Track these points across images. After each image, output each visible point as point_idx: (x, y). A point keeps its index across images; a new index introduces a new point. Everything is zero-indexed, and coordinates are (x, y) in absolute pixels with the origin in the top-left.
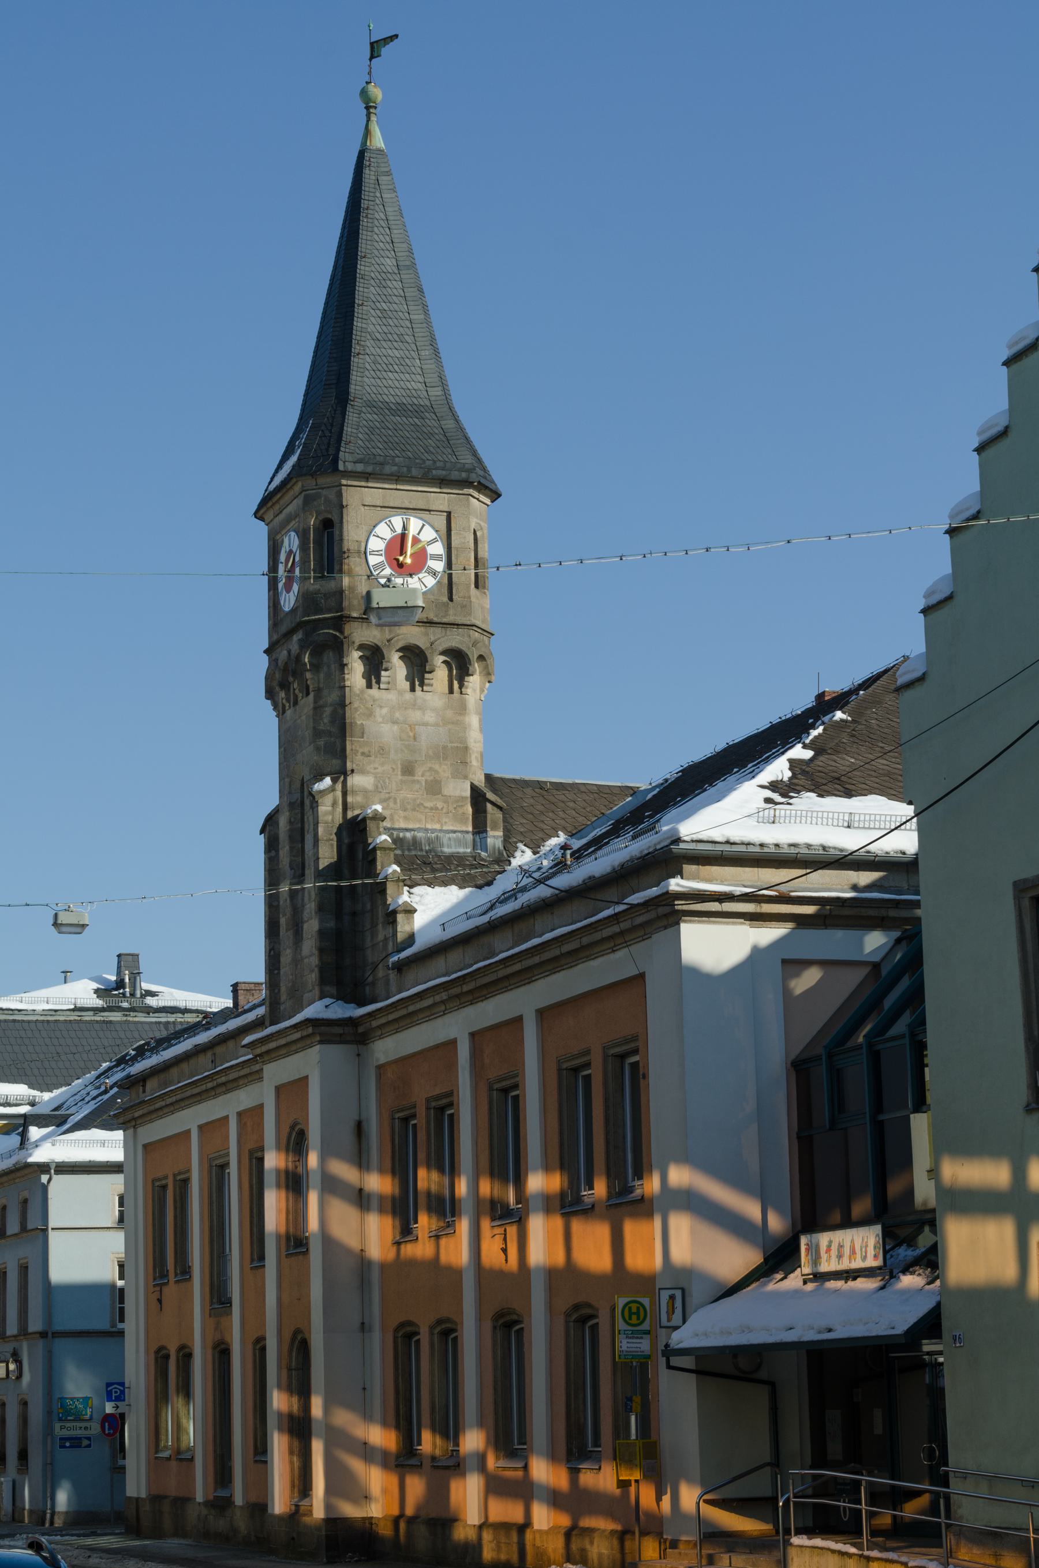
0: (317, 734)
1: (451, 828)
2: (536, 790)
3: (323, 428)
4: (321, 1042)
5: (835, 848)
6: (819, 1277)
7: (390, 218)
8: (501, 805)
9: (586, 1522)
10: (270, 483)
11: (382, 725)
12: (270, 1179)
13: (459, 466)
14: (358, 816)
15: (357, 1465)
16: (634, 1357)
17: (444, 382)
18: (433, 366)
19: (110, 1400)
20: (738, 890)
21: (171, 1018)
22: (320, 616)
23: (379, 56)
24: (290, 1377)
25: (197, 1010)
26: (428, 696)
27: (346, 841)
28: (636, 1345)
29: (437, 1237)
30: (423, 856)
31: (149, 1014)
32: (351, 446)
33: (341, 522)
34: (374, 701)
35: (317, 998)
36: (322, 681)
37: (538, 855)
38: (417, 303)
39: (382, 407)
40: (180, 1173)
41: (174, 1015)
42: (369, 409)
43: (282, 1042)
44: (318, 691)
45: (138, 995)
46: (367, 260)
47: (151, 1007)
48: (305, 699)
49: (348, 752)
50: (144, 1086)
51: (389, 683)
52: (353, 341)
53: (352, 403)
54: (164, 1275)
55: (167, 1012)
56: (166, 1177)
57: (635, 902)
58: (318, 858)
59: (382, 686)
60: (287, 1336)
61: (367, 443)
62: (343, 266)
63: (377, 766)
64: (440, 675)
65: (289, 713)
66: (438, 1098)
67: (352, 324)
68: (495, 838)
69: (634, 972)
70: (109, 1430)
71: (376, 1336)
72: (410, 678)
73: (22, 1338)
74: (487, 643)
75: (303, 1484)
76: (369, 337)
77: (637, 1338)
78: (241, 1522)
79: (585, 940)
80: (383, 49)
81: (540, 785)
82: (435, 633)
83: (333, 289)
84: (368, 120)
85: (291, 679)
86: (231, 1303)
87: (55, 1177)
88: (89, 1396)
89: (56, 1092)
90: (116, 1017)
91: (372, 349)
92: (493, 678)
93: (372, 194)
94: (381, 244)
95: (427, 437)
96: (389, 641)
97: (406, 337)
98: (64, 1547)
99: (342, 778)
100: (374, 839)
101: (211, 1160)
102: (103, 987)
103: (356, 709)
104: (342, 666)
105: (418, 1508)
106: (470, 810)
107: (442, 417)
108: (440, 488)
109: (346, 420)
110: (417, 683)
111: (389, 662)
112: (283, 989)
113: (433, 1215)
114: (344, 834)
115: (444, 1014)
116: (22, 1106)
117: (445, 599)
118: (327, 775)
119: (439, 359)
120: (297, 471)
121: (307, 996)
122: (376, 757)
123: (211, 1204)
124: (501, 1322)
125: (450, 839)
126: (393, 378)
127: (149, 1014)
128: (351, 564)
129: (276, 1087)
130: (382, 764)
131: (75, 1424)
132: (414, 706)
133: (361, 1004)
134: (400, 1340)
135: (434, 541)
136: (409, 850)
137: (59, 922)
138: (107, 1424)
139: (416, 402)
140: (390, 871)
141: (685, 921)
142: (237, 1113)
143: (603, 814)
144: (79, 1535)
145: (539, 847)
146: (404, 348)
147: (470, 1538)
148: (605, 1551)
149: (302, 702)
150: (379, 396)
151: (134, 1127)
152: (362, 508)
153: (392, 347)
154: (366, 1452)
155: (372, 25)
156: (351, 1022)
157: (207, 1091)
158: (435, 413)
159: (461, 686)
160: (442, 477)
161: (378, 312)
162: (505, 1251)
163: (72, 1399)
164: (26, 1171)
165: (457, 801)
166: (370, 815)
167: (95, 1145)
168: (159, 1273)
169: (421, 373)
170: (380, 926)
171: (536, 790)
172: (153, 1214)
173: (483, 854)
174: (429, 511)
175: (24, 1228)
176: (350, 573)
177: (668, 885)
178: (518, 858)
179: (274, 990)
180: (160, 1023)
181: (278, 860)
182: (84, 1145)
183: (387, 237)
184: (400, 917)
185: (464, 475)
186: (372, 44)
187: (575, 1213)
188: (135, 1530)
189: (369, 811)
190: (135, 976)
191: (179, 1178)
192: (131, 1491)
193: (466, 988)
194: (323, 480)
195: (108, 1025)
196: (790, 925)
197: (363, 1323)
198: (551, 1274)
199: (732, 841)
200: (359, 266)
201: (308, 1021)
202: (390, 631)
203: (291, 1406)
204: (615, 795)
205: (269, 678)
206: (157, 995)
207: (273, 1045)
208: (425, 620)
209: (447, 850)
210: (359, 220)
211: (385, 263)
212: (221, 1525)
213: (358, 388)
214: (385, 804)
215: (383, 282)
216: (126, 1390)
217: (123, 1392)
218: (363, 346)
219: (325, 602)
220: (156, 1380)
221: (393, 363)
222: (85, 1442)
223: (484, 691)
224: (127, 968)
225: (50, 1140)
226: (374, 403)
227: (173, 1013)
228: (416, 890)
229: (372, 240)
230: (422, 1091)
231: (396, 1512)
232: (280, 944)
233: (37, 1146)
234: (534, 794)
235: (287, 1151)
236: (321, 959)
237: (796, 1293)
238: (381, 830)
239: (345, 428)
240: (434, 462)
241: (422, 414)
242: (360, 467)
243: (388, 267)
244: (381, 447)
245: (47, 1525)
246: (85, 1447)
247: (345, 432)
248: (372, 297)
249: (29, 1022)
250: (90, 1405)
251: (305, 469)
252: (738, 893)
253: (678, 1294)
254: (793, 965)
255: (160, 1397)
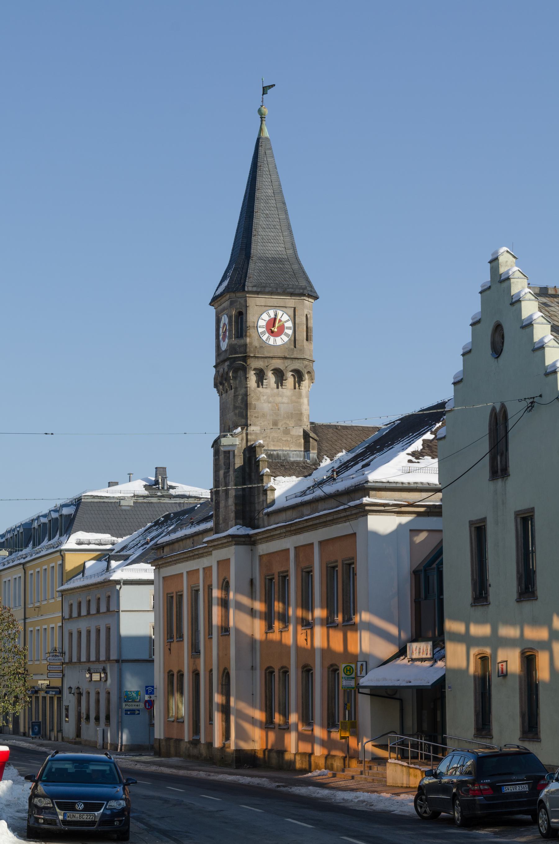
0: (235, 408)
1: (294, 449)
2: (334, 430)
3: (239, 270)
4: (235, 544)
5: (433, 484)
6: (413, 660)
7: (271, 170)
8: (316, 439)
9: (333, 753)
10: (217, 290)
11: (264, 404)
12: (215, 601)
13: (299, 287)
14: (253, 444)
15: (247, 726)
16: (348, 688)
17: (294, 246)
18: (289, 240)
19: (147, 693)
20: (392, 502)
21: (182, 501)
22: (237, 356)
23: (267, 94)
24: (222, 688)
25: (195, 496)
26: (284, 391)
27: (247, 456)
28: (349, 683)
29: (281, 632)
30: (281, 462)
31: (171, 498)
32: (251, 279)
33: (246, 313)
34: (260, 393)
35: (234, 525)
36: (237, 384)
37: (333, 461)
38: (282, 210)
39: (266, 259)
40: (179, 592)
41: (183, 499)
42: (259, 261)
43: (220, 542)
44: (236, 388)
45: (166, 489)
46: (260, 190)
47: (172, 495)
48: (230, 391)
49: (248, 416)
50: (163, 550)
51: (267, 385)
52: (253, 229)
53: (252, 258)
54: (172, 638)
55: (180, 498)
56: (173, 593)
57: (351, 505)
58: (235, 464)
59: (264, 387)
60: (221, 670)
61: (258, 277)
62: (249, 193)
63: (261, 422)
64: (290, 380)
65: (224, 395)
66: (283, 572)
67: (253, 221)
68: (313, 454)
69: (351, 532)
70: (148, 706)
71: (258, 672)
72: (277, 383)
73: (107, 662)
74: (311, 366)
75: (227, 736)
76: (260, 227)
77: (349, 680)
78: (203, 751)
79: (335, 517)
80: (268, 91)
81: (336, 427)
82: (287, 362)
83: (243, 210)
84: (262, 123)
85: (224, 382)
86: (200, 653)
87: (123, 587)
88: (139, 690)
89: (125, 538)
90: (154, 500)
91: (261, 232)
92: (314, 381)
93: (262, 159)
94: (266, 183)
95: (285, 273)
96: (267, 366)
97: (277, 226)
98: (125, 761)
99: (246, 428)
100: (260, 455)
101: (192, 587)
102: (148, 484)
103: (252, 397)
104: (246, 378)
105: (272, 746)
106: (303, 441)
107: (292, 263)
108: (291, 297)
109: (249, 267)
110: (280, 385)
111: (267, 376)
112: (221, 518)
113: (280, 622)
114: (247, 452)
115: (285, 537)
116: (108, 545)
117: (293, 347)
118: (239, 426)
119: (292, 235)
120: (228, 290)
121: (230, 523)
122: (261, 418)
123: (192, 607)
124: (305, 669)
125: (293, 454)
126: (271, 246)
127: (171, 498)
128: (251, 332)
130: (264, 421)
131: (132, 703)
132: (278, 395)
133: (254, 528)
134: (267, 674)
135: (288, 321)
136: (275, 459)
137: (121, 505)
138: (147, 704)
139: (281, 257)
140: (265, 471)
141: (370, 515)
142: (203, 568)
143: (364, 440)
144: (133, 756)
145: (334, 457)
146: (276, 232)
147: (292, 759)
148: (339, 764)
149: (229, 392)
150: (264, 254)
151: (159, 568)
152: (256, 307)
153: (271, 231)
154: (253, 721)
155: (263, 79)
156: (248, 536)
157: (190, 556)
158: (289, 262)
159: (299, 386)
160: (291, 292)
161: (264, 215)
162: (306, 640)
163: (131, 692)
164: (109, 583)
165: (297, 437)
166: (258, 445)
167: (142, 571)
168: (169, 636)
169: (283, 243)
170: (261, 494)
171: (334, 430)
172: (167, 612)
173: (308, 461)
174: (286, 307)
175: (108, 610)
176: (250, 336)
177: (362, 500)
178: (323, 463)
180: (176, 503)
181: (219, 460)
182: (137, 571)
183: (269, 179)
184: (269, 492)
185: (301, 291)
186: (263, 88)
187: (331, 627)
188: (158, 754)
189: (257, 443)
190: (164, 479)
191: (178, 594)
192: (157, 736)
193: (292, 529)
194: (239, 294)
195: (151, 504)
196: (415, 515)
197: (252, 666)
198: (323, 650)
199: (390, 482)
200: (256, 194)
201: (229, 536)
202: (268, 362)
203: (222, 701)
204: (369, 431)
205: (215, 379)
206: (175, 488)
207: (216, 543)
208: (283, 357)
209: (292, 459)
210: (257, 172)
211: (267, 192)
212: (195, 752)
213: (255, 251)
214: (265, 439)
215: (267, 201)
216: (155, 689)
217: (153, 690)
218: (257, 231)
219: (239, 349)
220: (168, 685)
221: (271, 239)
222: (137, 712)
223: (310, 387)
224: (160, 474)
225: (121, 569)
226: (262, 258)
227: (183, 498)
228: (277, 478)
229: (263, 181)
230: (277, 569)
231: (265, 748)
232: (219, 497)
233: (114, 572)
234: (333, 432)
235: (222, 589)
236: (236, 508)
237: (405, 665)
238: (262, 451)
239: (248, 271)
240: (288, 285)
241: (283, 262)
242: (255, 289)
243: (269, 194)
244: (264, 279)
245: (119, 750)
246: (137, 714)
247: (248, 272)
248: (262, 208)
249: (111, 503)
250: (139, 695)
251: (231, 289)
252: (391, 504)
253: (364, 663)
254: (415, 532)
255: (170, 692)
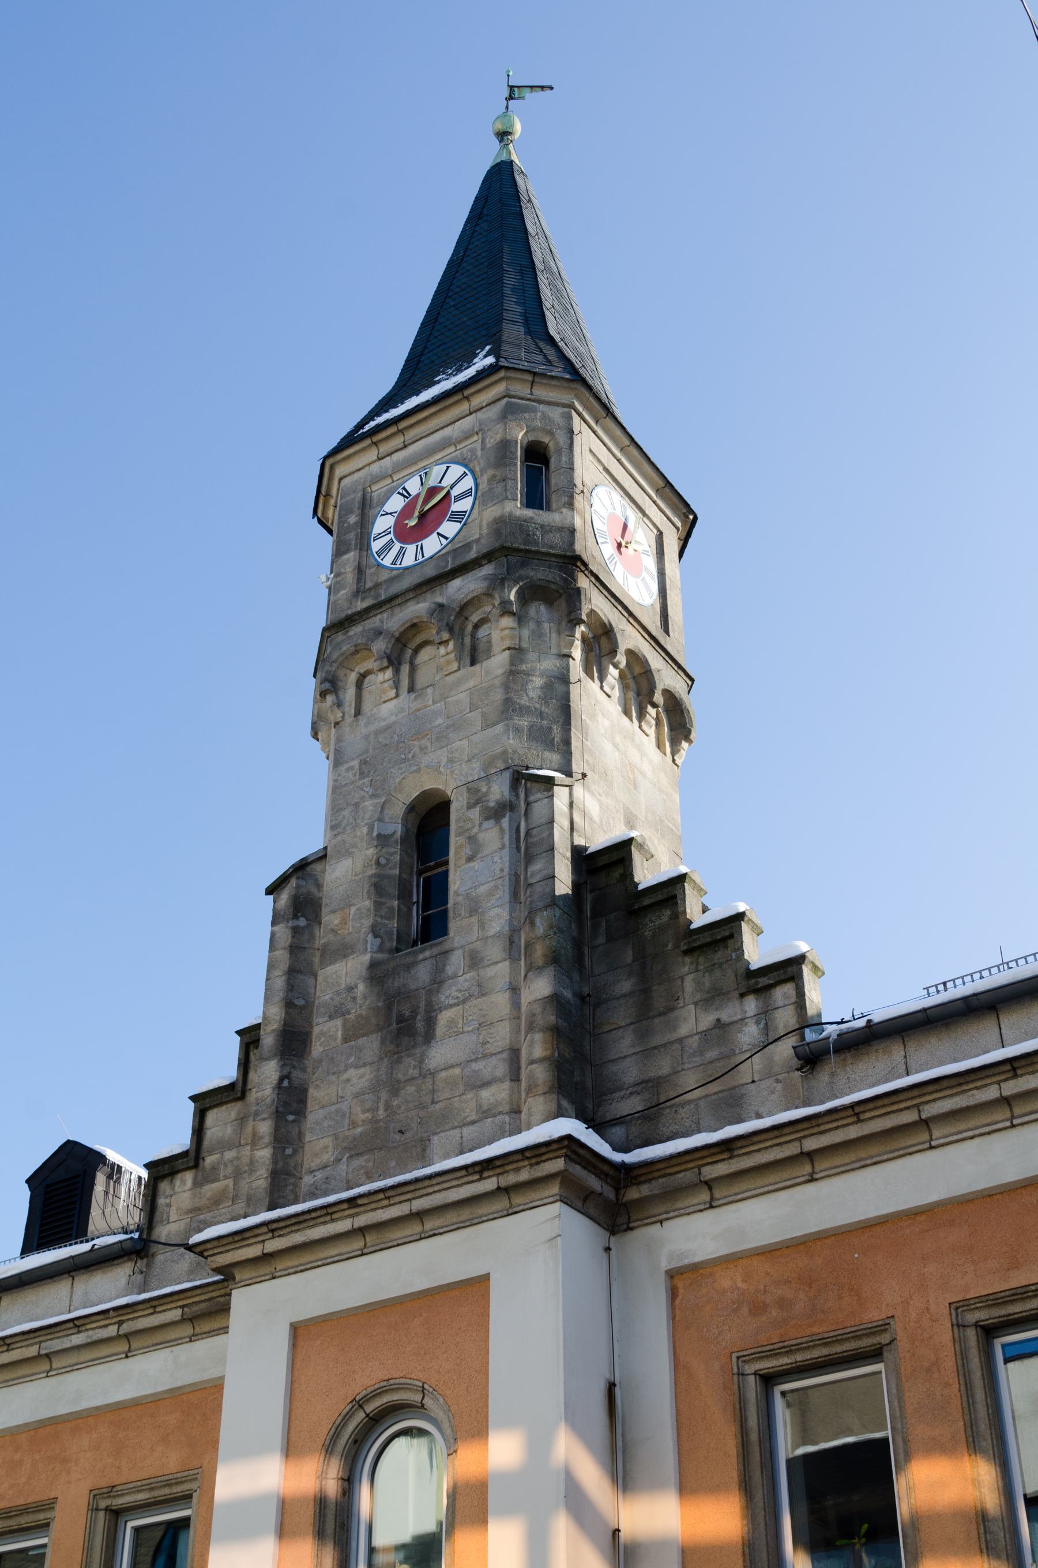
129: (292, 1325)
179: (284, 1150)
